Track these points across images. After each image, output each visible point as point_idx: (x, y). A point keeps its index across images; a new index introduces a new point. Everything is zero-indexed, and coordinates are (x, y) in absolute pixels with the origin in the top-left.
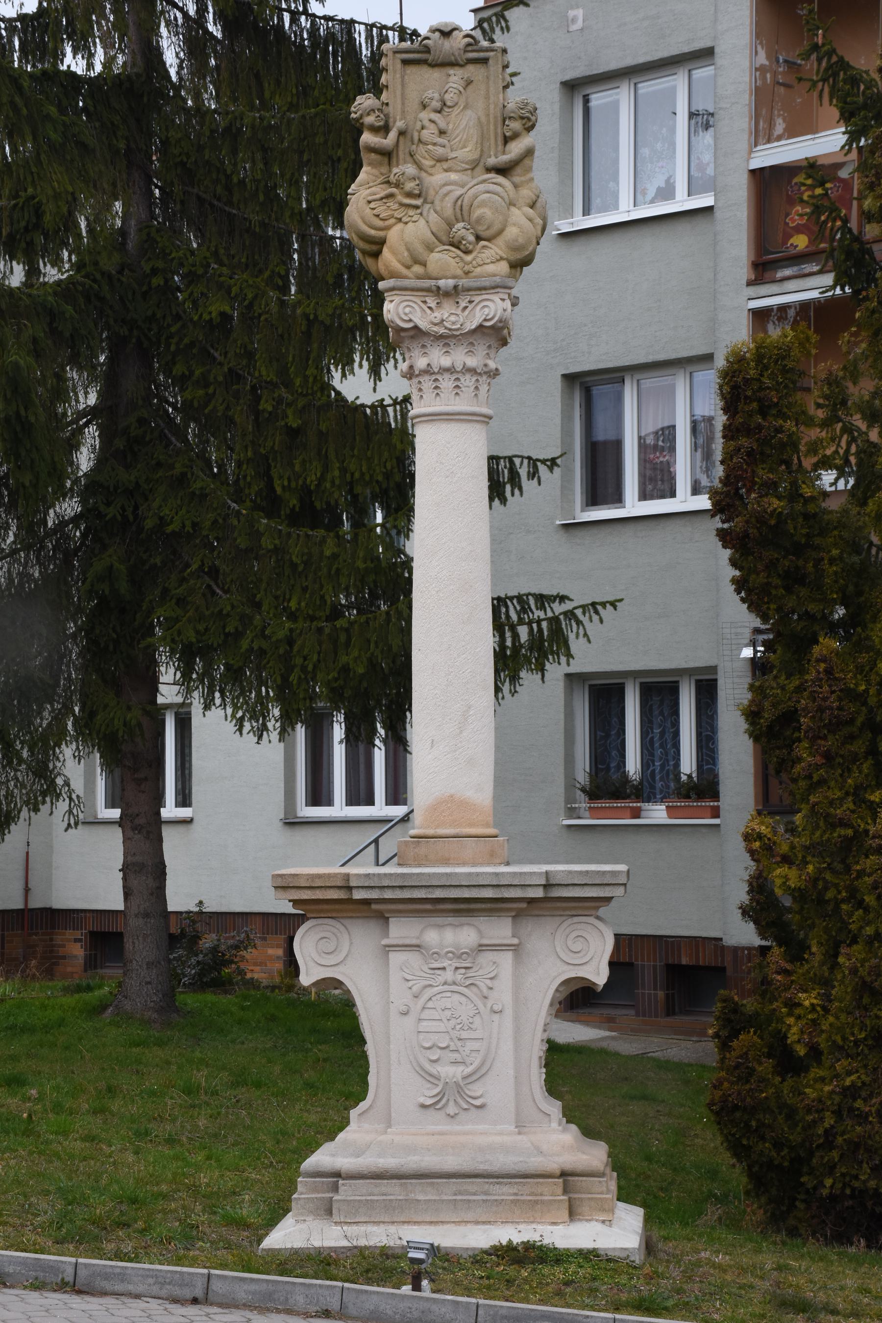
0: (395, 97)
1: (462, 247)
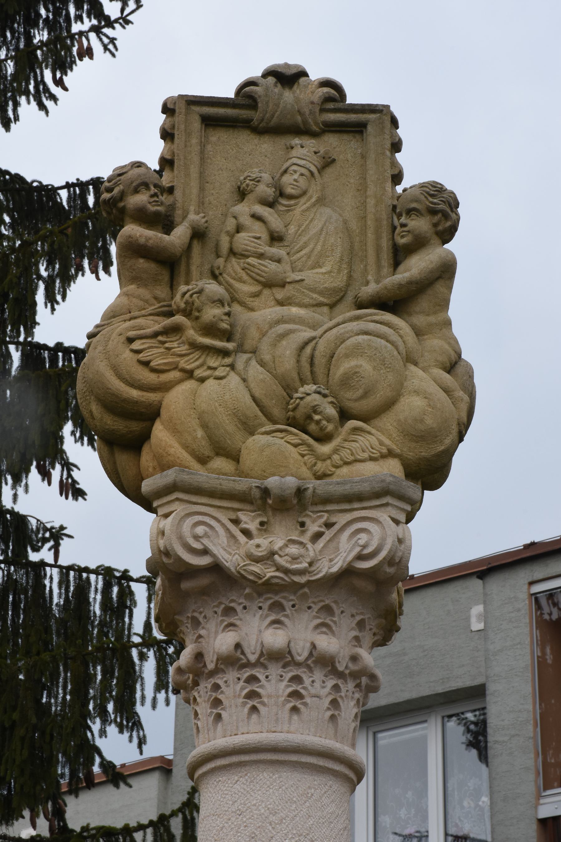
0: (188, 175)
1: (312, 427)
